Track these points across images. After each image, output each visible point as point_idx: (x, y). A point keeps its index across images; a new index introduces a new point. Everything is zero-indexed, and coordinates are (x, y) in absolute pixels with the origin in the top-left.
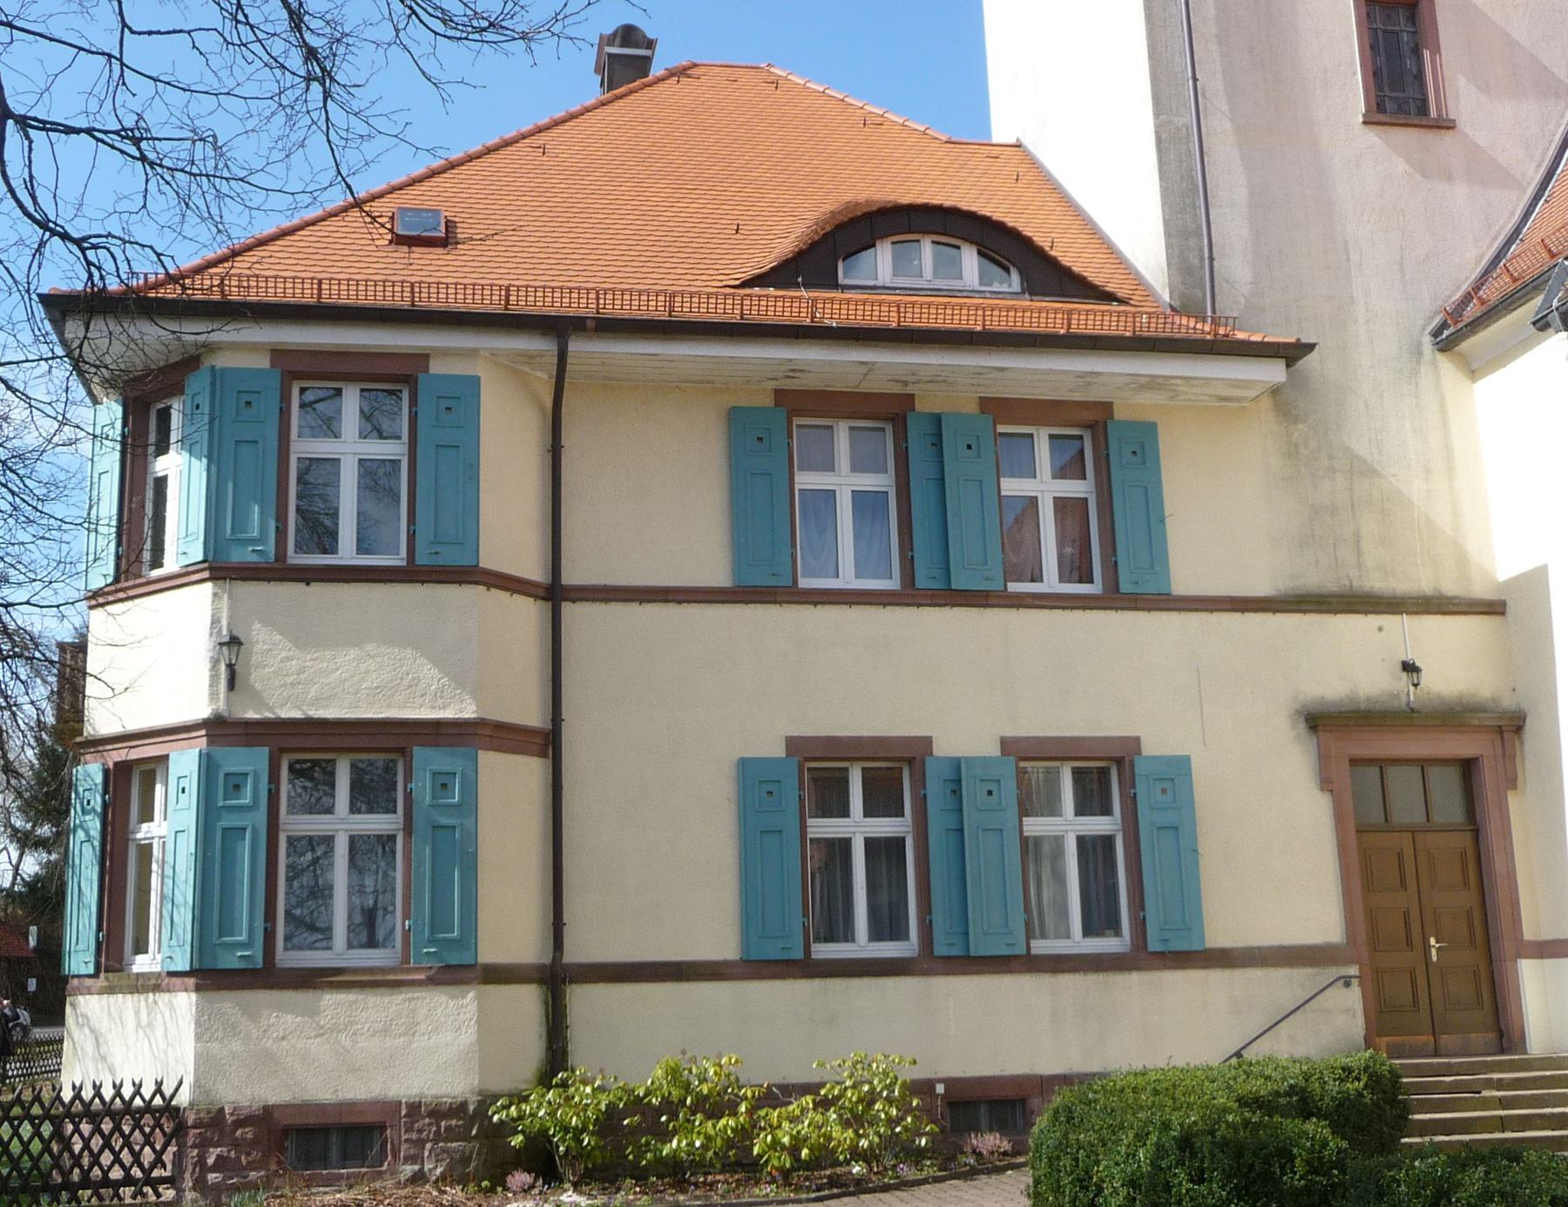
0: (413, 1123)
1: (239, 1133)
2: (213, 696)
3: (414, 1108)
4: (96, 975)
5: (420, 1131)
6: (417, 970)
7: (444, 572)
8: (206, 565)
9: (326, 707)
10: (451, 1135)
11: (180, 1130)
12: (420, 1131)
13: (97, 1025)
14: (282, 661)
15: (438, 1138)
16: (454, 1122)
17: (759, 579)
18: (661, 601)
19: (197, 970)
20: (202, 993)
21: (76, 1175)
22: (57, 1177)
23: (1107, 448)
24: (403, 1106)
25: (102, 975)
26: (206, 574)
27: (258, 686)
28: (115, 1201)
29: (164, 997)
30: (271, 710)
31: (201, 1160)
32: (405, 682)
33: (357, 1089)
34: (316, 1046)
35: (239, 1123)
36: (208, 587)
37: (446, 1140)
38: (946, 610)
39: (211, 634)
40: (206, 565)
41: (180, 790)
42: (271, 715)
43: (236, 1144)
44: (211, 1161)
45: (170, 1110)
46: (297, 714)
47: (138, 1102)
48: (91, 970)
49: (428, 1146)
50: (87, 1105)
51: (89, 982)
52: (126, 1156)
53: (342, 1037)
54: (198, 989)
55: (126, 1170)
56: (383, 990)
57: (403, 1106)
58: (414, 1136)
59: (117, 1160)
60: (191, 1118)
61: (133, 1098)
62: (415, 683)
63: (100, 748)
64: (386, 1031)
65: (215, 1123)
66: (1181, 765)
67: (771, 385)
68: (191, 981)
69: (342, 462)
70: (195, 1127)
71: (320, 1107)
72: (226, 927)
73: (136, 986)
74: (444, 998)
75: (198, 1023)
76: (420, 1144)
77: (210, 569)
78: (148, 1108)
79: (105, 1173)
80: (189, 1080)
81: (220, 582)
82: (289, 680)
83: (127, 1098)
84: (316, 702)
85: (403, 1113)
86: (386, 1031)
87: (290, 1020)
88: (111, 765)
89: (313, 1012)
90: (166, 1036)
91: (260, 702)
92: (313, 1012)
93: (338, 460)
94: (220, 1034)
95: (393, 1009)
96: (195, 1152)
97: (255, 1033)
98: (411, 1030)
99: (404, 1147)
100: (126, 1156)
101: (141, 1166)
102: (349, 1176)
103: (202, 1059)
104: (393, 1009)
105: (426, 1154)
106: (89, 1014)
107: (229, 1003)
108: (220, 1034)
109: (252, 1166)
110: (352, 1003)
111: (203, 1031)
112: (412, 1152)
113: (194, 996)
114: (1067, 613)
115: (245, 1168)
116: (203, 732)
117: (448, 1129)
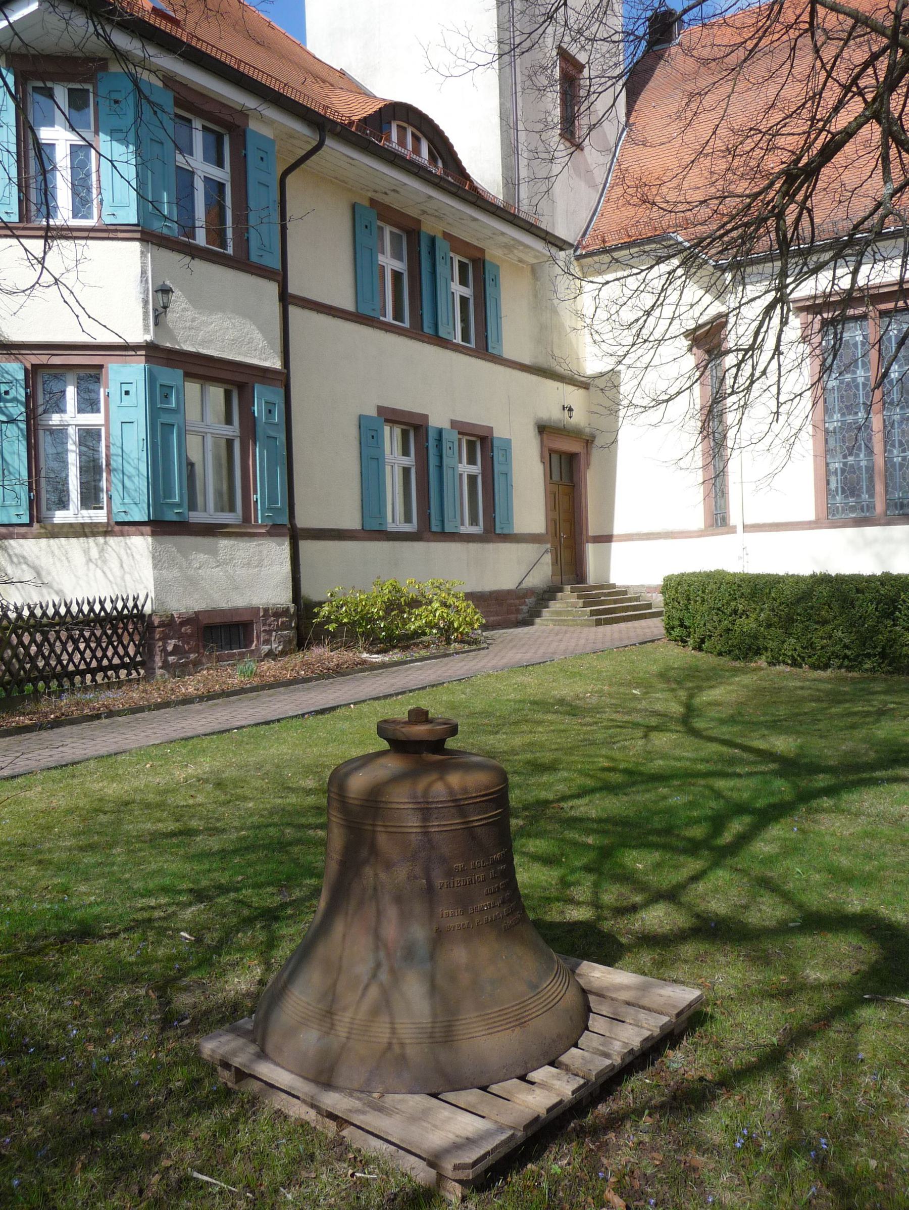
0: (266, 620)
1: (183, 630)
2: (146, 329)
3: (266, 610)
4: (30, 525)
5: (270, 625)
6: (260, 526)
7: (260, 268)
8: (140, 228)
9: (208, 348)
10: (284, 626)
11: (150, 627)
12: (270, 625)
13: (37, 562)
14: (183, 311)
15: (279, 629)
16: (284, 619)
17: (366, 310)
18: (326, 314)
19: (153, 521)
20: (159, 538)
21: (94, 664)
22: (71, 668)
23: (484, 273)
24: (261, 610)
25: (35, 524)
26: (138, 235)
27: (171, 325)
28: (106, 680)
29: (112, 540)
30: (178, 344)
31: (164, 650)
32: (246, 340)
33: (240, 601)
34: (218, 573)
35: (184, 623)
36: (136, 245)
37: (281, 630)
38: (426, 345)
39: (141, 281)
40: (140, 228)
41: (123, 393)
42: (177, 347)
43: (181, 637)
44: (170, 648)
45: (141, 616)
46: (192, 349)
47: (126, 612)
48: (25, 519)
49: (274, 633)
50: (97, 616)
51: (23, 530)
52: (121, 650)
53: (229, 568)
54: (154, 534)
55: (121, 658)
56: (246, 538)
57: (261, 610)
58: (267, 628)
59: (116, 652)
60: (156, 621)
61: (123, 609)
62: (251, 341)
63: (13, 352)
64: (249, 564)
65: (170, 625)
66: (508, 442)
67: (370, 194)
68: (148, 529)
69: (57, 147)
70: (158, 627)
71: (222, 612)
72: (168, 493)
73: (84, 532)
74: (274, 545)
75: (154, 558)
76: (269, 632)
77: (142, 232)
78: (131, 616)
79: (110, 661)
80: (152, 594)
81: (145, 243)
82: (188, 324)
83: (120, 610)
84: (203, 343)
85: (261, 614)
86: (249, 564)
87: (202, 557)
88: (29, 367)
89: (214, 552)
90: (122, 566)
91: (173, 338)
92: (214, 552)
93: (54, 145)
94: (166, 565)
95: (252, 550)
96: (160, 643)
97: (185, 565)
98: (260, 565)
99: (263, 634)
100: (121, 650)
101: (129, 656)
102: (240, 654)
103: (158, 582)
104: (252, 550)
105: (273, 639)
106: (25, 554)
107: (172, 543)
108: (166, 565)
109: (191, 651)
110: (232, 546)
111: (157, 563)
112: (267, 637)
113: (150, 539)
114: (470, 358)
115: (186, 652)
116: (143, 353)
117: (283, 623)
